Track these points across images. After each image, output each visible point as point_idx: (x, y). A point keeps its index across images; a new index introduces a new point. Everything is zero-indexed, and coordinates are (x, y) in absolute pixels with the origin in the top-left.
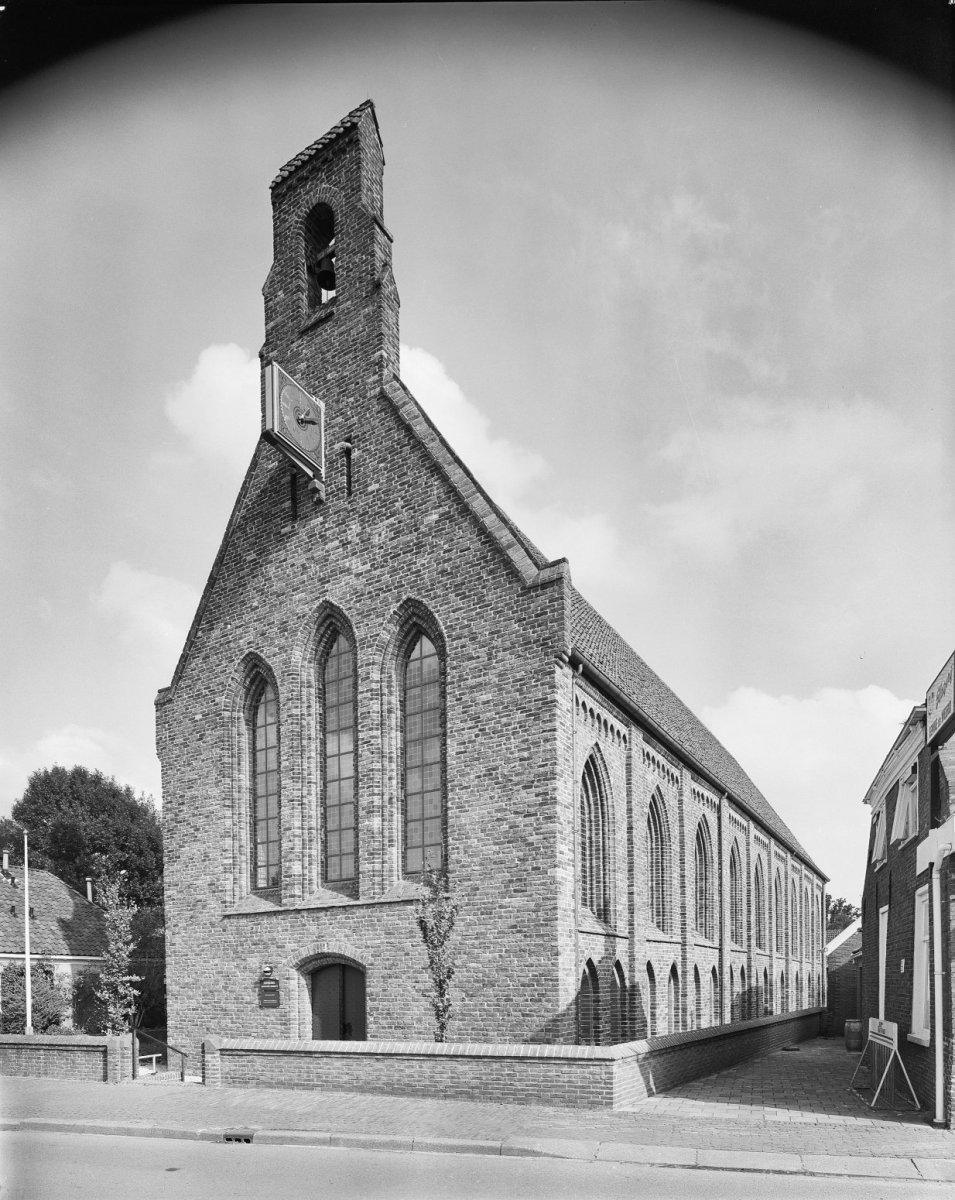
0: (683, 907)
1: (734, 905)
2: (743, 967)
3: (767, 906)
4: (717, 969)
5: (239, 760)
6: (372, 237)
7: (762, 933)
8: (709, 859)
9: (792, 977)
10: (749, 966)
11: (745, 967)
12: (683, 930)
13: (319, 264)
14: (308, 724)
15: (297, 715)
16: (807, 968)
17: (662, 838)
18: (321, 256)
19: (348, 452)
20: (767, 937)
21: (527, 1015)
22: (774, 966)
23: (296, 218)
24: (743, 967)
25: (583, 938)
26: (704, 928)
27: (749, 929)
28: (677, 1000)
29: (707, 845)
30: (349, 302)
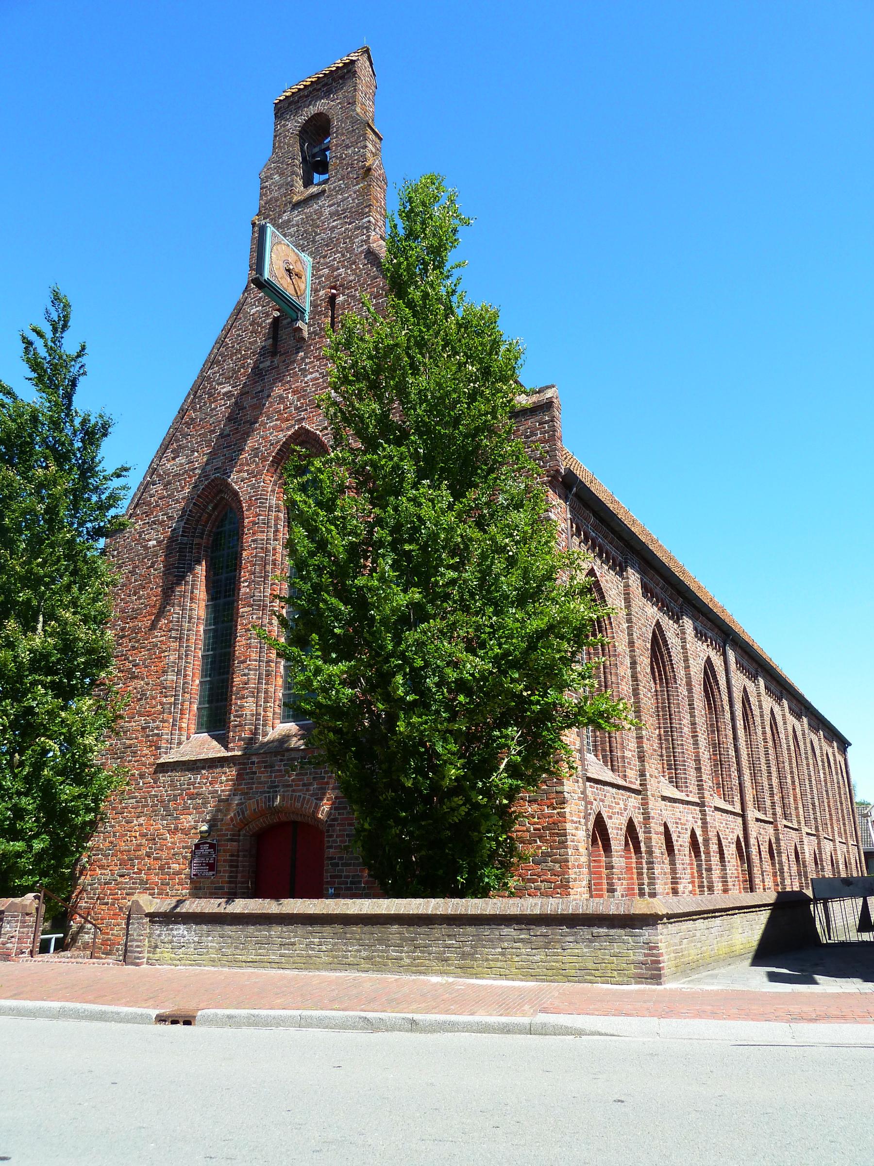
0: (698, 761)
1: (753, 766)
2: (770, 841)
3: (787, 768)
4: (742, 840)
5: (193, 588)
6: (364, 136)
7: (786, 801)
8: (719, 709)
9: (826, 857)
10: (778, 840)
11: (773, 841)
12: (700, 788)
13: (314, 156)
14: (274, 549)
15: (263, 540)
16: (841, 849)
17: (666, 679)
18: (316, 150)
19: (333, 298)
20: (793, 806)
21: (529, 881)
22: (805, 843)
23: (294, 124)
24: (770, 841)
25: (591, 787)
26: (721, 787)
27: (772, 795)
28: (700, 876)
29: (716, 693)
30: (342, 182)
